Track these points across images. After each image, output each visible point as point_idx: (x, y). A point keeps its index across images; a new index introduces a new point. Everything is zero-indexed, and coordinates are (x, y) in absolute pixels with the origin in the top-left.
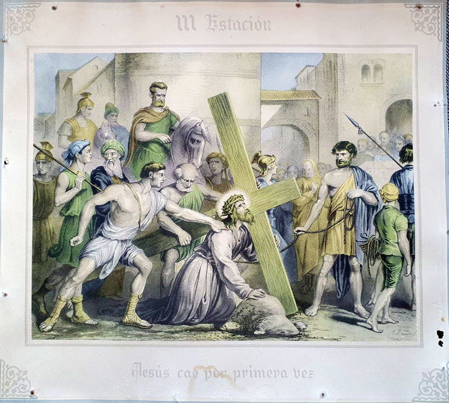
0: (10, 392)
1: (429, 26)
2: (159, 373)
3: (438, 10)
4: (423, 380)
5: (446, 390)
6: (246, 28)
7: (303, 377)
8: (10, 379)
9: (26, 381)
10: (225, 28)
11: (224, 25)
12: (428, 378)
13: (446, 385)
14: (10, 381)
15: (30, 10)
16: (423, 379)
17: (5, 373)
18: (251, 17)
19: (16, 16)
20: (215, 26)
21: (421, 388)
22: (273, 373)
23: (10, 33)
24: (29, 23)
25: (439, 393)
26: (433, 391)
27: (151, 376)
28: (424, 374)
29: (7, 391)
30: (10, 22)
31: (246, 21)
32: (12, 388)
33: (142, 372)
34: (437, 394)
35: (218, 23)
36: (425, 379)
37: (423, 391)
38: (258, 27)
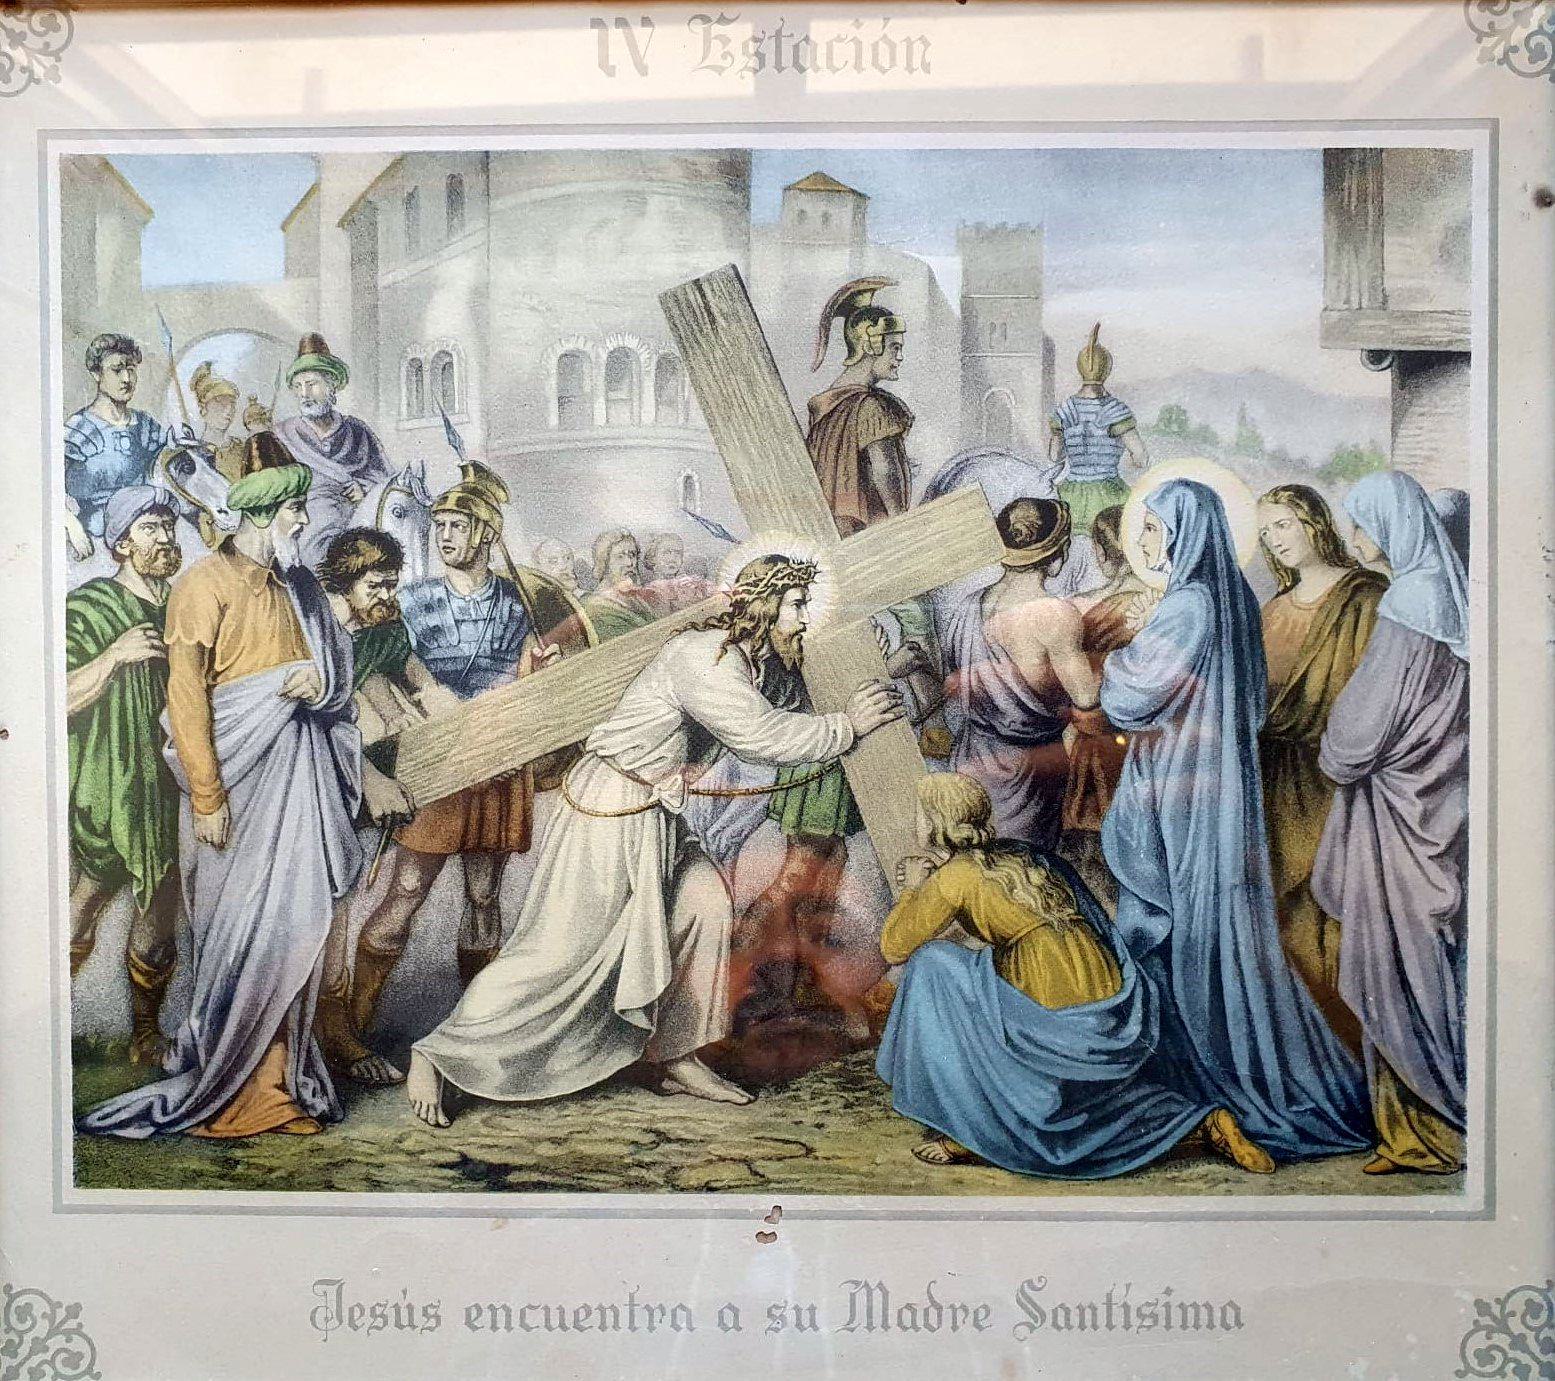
2: (404, 1313)
12: (1494, 1318)
16: (1476, 1322)
20: (724, 56)
25: (1528, 1368)
26: (1507, 1360)
27: (378, 1328)
31: (839, 39)
33: (345, 1314)
36: (1486, 1321)
37: (1474, 1363)
38: (885, 61)
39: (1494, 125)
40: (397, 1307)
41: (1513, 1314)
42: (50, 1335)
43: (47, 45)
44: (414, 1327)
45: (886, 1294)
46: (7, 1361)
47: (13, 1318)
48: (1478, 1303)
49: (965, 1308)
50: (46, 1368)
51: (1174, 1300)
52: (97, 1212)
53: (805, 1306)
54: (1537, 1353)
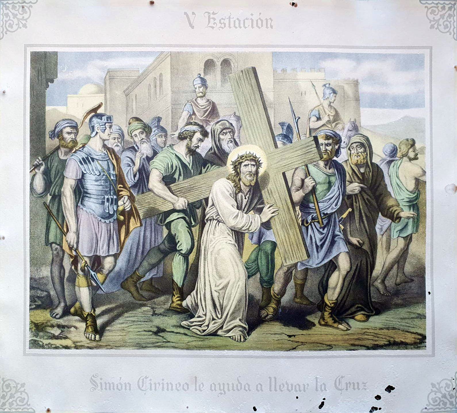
0: (7, 406)
1: (445, 24)
3: (454, 7)
4: (26, 20)
5: (453, 400)
6: (246, 26)
9: (432, 19)
10: (225, 26)
11: (221, 24)
12: (437, 389)
13: (5, 16)
14: (7, 395)
17: (452, 27)
18: (252, 15)
20: (214, 24)
21: (29, 13)
23: (5, 30)
24: (25, 20)
25: (446, 403)
28: (433, 385)
30: (5, 19)
31: (247, 19)
33: (319, 387)
35: (217, 21)
38: (260, 25)
41: (442, 387)
43: (23, 17)
46: (2, 401)
48: (26, 27)
50: (441, 10)
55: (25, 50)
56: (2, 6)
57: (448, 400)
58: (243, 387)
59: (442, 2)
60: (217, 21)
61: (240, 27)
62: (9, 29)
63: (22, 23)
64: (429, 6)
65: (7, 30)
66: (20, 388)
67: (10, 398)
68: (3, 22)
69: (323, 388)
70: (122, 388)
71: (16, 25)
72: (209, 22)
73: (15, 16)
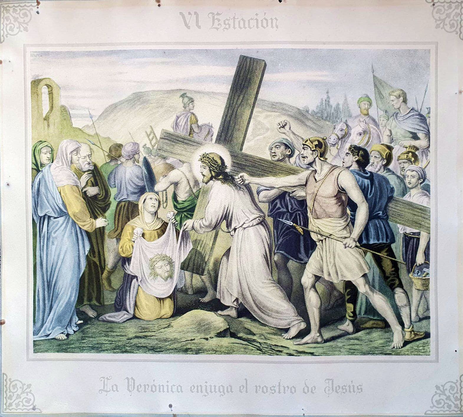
0: (14, 406)
1: (451, 23)
6: (252, 26)
7: (336, 391)
8: (13, 393)
14: (453, 17)
15: (26, 9)
18: (257, 14)
19: (12, 16)
20: (219, 25)
22: (195, 390)
23: (6, 33)
24: (26, 23)
25: (451, 405)
26: (445, 403)
29: (11, 404)
31: (252, 19)
32: (15, 403)
33: (334, 388)
34: (449, 406)
35: (222, 22)
37: (435, 404)
38: (265, 25)
39: (437, 43)
40: (349, 387)
41: (446, 389)
42: (445, 395)
44: (354, 391)
45: (134, 380)
47: (11, 388)
48: (30, 385)
49: (288, 387)
50: (447, 9)
51: (208, 384)
52: (404, 362)
53: (213, 385)
54: (454, 401)
55: (25, 51)
56: (2, 9)
57: (453, 402)
58: (310, 390)
59: (2, 20)
60: (222, 22)
61: (245, 28)
62: (10, 32)
63: (23, 27)
64: (6, 33)
65: (8, 34)
66: (26, 389)
67: (17, 398)
68: (4, 25)
69: (229, 390)
70: (156, 390)
71: (17, 28)
72: (213, 24)
73: (16, 19)
